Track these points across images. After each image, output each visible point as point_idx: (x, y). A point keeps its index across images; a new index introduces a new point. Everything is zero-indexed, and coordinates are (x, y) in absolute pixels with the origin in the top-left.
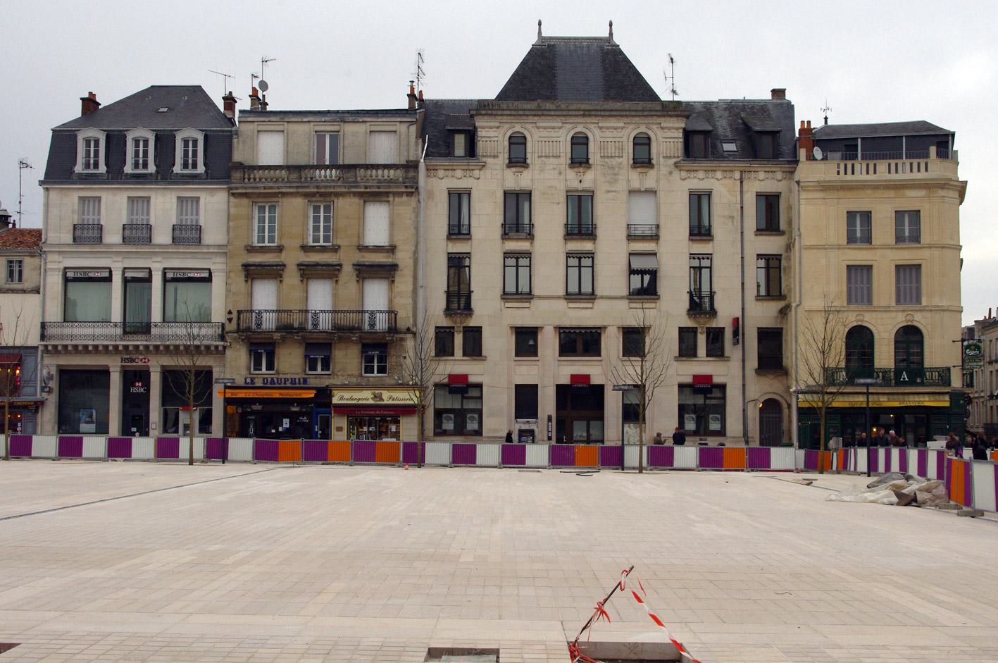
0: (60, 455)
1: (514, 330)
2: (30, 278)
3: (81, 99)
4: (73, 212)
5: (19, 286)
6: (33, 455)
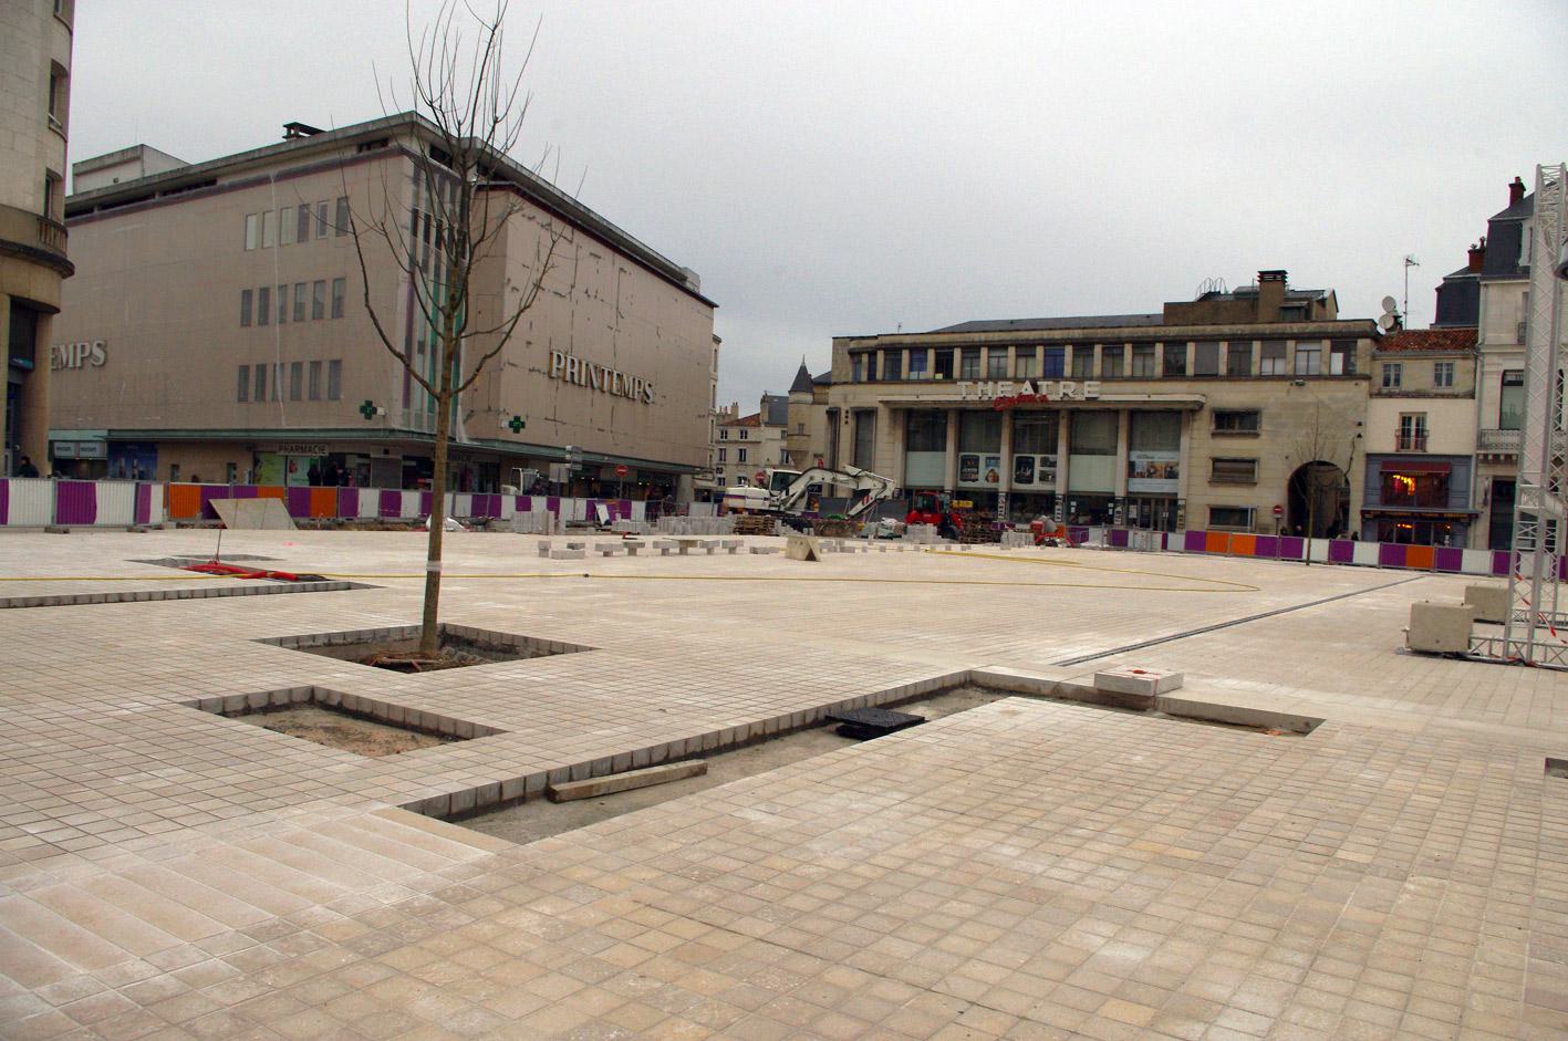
0: (1495, 571)
1: (901, 418)
2: (1461, 381)
3: (1518, 179)
4: (1516, 310)
5: (1448, 390)
6: (1355, 561)
